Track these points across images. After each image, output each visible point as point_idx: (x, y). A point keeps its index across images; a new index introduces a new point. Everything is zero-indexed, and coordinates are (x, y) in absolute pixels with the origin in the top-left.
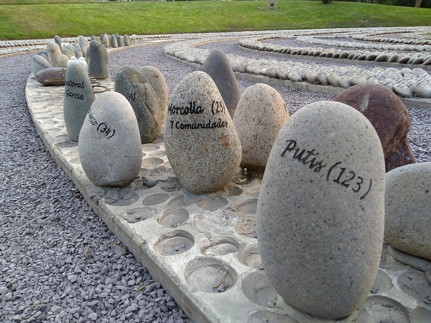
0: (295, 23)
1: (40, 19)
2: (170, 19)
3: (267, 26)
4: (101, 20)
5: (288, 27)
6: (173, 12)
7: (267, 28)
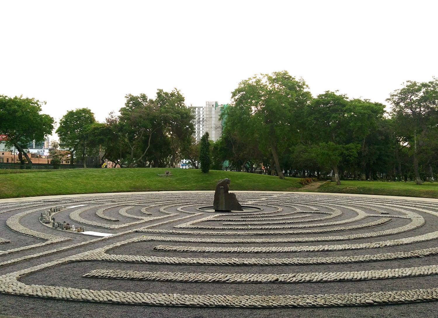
0: (178, 186)
1: (7, 186)
2: (94, 183)
3: (159, 188)
4: (46, 185)
5: (172, 189)
6: (97, 178)
7: (159, 189)
